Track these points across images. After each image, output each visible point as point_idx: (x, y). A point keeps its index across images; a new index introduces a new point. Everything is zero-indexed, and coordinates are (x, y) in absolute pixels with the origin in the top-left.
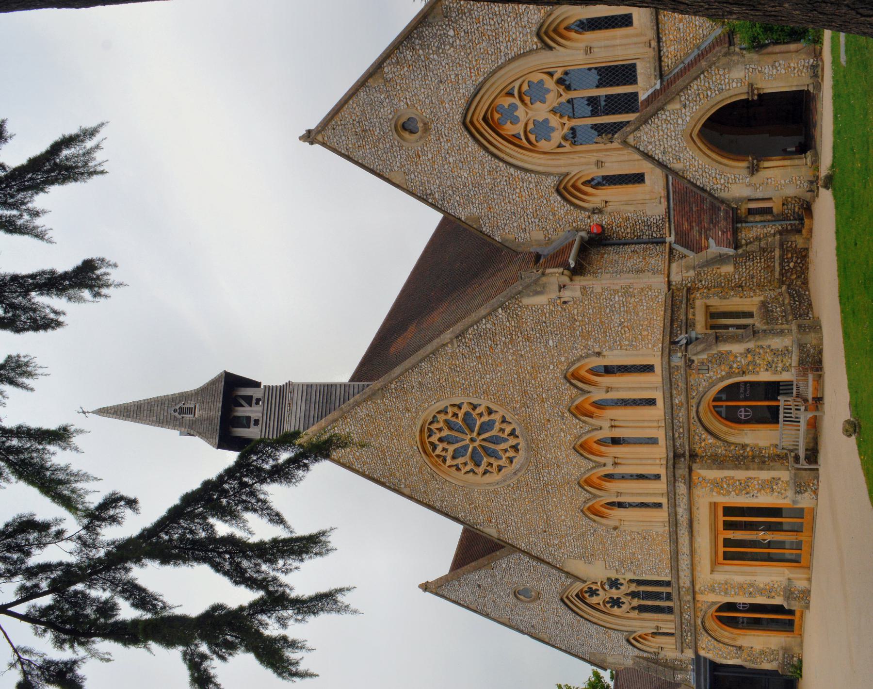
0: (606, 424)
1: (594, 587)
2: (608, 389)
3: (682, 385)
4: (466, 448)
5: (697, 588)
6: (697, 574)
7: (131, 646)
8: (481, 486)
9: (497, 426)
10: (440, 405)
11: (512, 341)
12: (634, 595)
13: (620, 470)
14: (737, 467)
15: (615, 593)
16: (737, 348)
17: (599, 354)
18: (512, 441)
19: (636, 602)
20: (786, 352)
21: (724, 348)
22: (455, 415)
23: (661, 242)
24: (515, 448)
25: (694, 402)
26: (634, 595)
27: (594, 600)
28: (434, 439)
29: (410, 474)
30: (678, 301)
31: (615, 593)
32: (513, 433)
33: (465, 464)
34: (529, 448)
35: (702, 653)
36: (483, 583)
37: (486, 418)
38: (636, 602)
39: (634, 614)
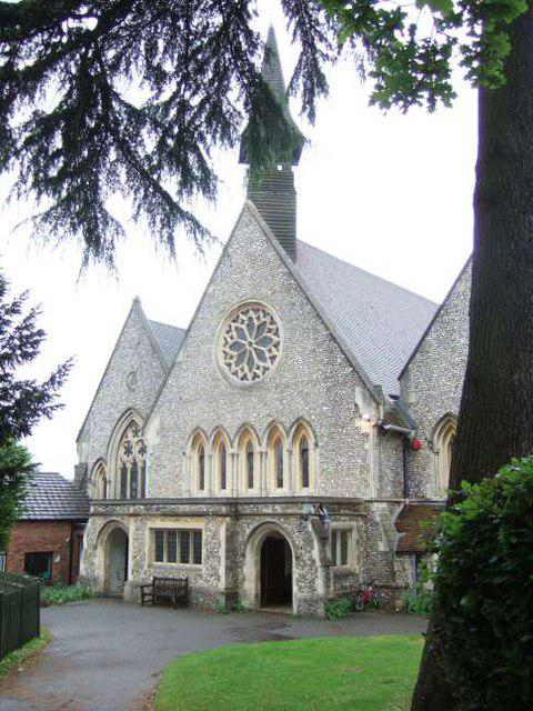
0: (263, 449)
1: (140, 434)
2: (290, 452)
3: (289, 511)
4: (244, 338)
7: (246, 189)
8: (215, 349)
9: (262, 364)
10: (277, 319)
11: (326, 377)
13: (229, 459)
14: (227, 551)
16: (316, 554)
17: (316, 445)
18: (250, 376)
19: (129, 466)
20: (313, 589)
21: (316, 544)
22: (270, 331)
23: (406, 494)
24: (244, 377)
25: (275, 520)
26: (135, 464)
27: (130, 434)
28: (251, 314)
30: (352, 507)
31: (135, 450)
32: (256, 376)
33: (232, 338)
34: (244, 388)
37: (267, 355)
38: (129, 466)
39: (120, 465)
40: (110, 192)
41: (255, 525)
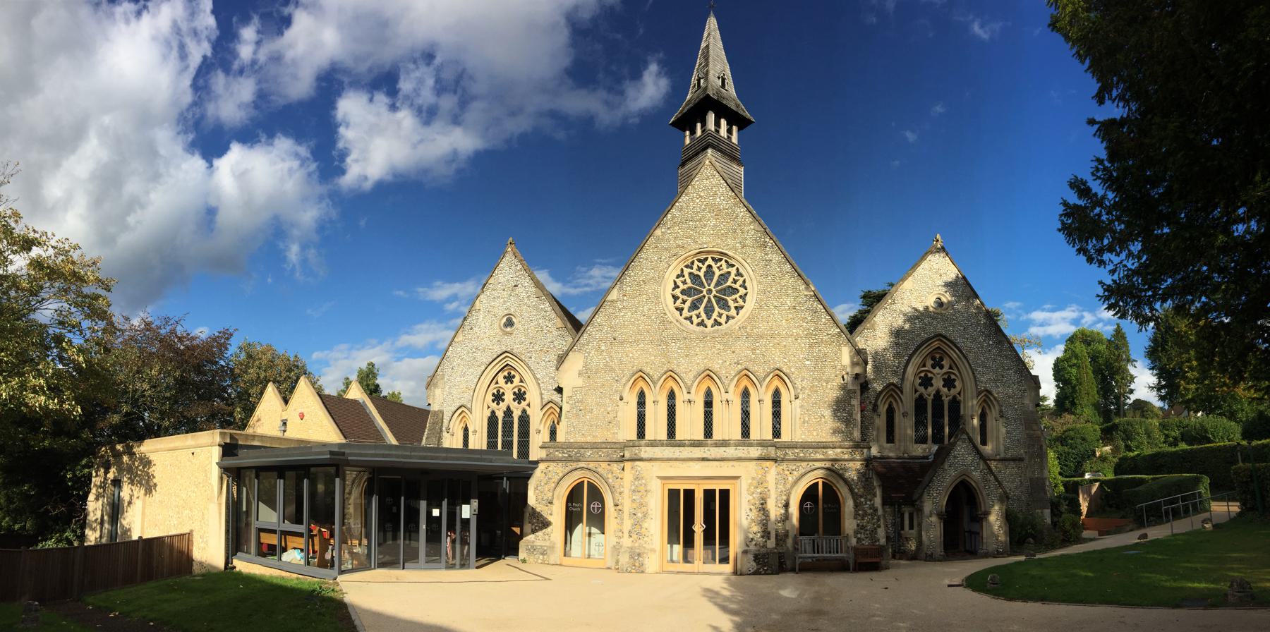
5: (638, 463)
6: (657, 464)
9: (704, 316)
12: (508, 412)
15: (509, 397)
19: (500, 415)
26: (508, 412)
29: (675, 238)
31: (509, 397)
35: (542, 466)
36: (520, 289)
38: (500, 415)
40: (56, 239)
41: (802, 471)
